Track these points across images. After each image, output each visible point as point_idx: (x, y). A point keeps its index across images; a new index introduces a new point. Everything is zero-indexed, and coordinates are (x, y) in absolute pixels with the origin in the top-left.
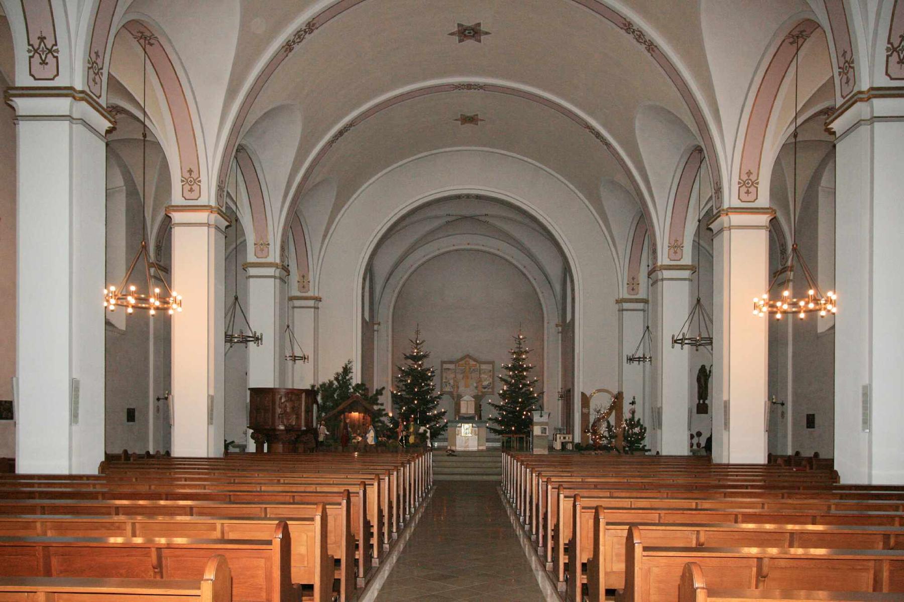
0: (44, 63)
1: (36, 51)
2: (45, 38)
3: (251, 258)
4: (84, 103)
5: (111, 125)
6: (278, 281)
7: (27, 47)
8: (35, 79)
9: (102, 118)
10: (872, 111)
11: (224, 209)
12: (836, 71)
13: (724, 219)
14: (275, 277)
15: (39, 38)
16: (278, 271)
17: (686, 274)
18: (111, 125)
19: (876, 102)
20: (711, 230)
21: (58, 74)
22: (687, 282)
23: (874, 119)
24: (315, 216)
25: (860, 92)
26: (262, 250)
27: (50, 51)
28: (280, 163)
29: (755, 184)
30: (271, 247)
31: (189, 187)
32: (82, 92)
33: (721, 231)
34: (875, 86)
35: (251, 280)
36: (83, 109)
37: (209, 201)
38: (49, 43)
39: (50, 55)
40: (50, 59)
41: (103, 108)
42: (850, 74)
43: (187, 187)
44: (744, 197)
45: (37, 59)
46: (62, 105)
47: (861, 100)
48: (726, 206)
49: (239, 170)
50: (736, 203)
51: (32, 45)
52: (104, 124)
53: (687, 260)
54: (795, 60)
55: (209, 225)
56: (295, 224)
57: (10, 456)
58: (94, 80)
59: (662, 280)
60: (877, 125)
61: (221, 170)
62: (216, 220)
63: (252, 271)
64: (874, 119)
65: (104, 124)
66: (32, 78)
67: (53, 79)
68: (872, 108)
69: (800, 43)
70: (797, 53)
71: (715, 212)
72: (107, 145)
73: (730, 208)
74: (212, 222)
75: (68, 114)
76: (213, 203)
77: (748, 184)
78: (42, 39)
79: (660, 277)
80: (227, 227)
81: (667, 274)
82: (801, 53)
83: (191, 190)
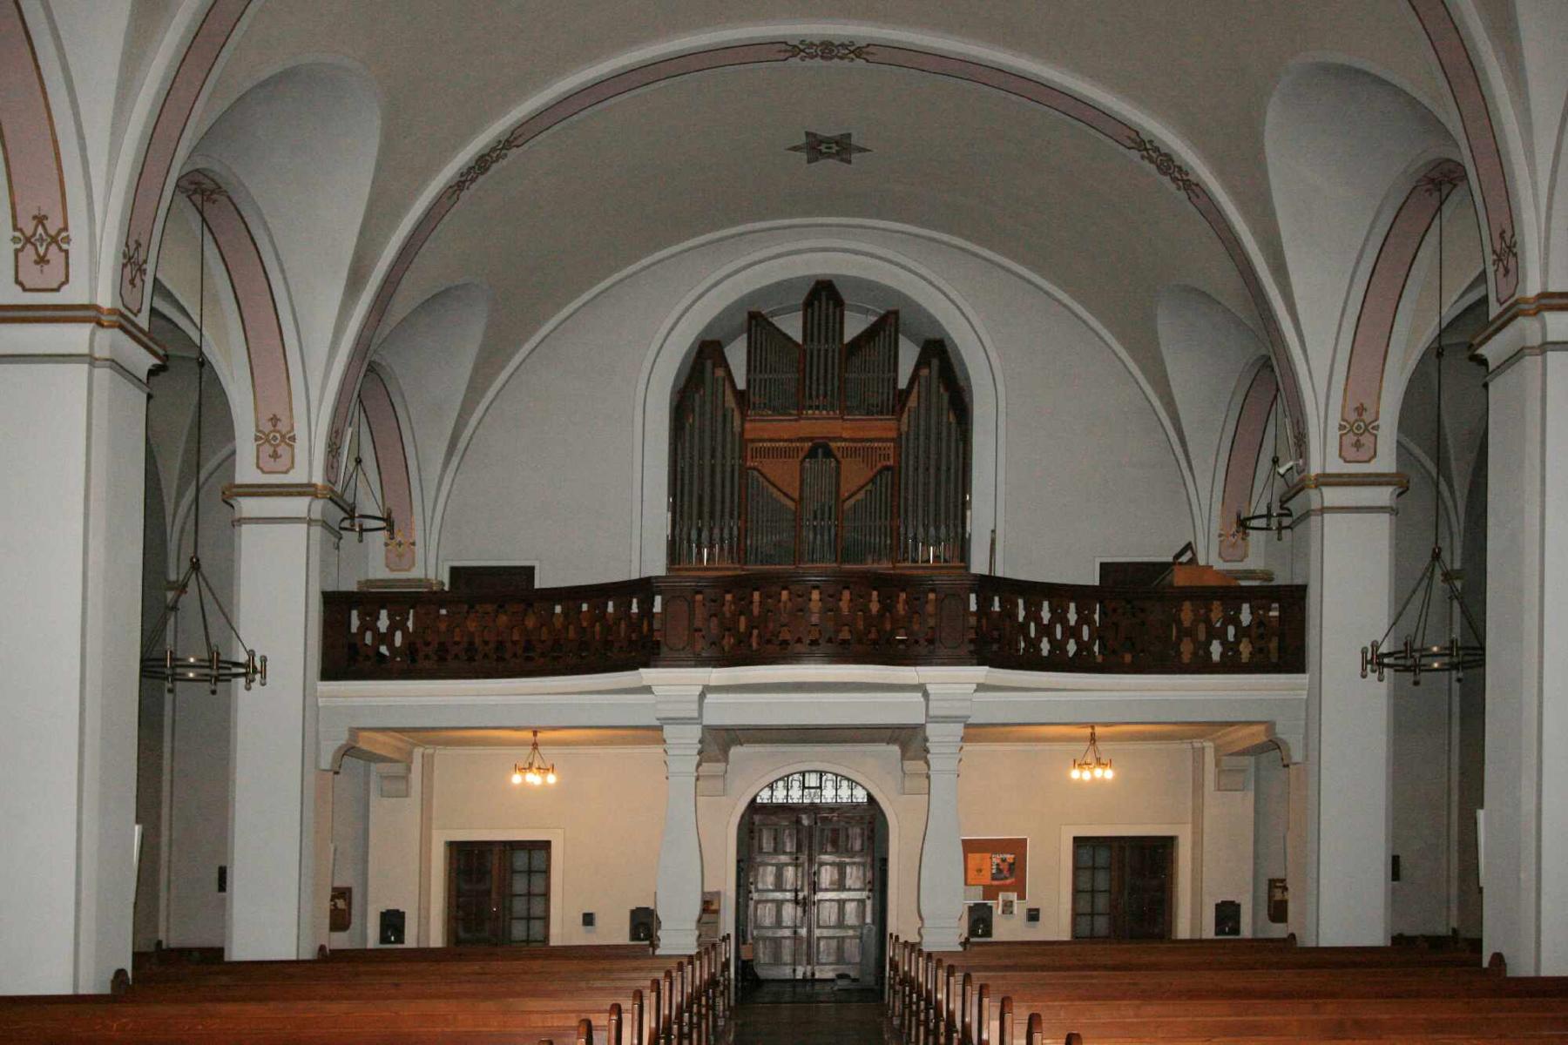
0: (42, 260)
1: (28, 240)
2: (46, 217)
3: (247, 472)
4: (117, 331)
5: (157, 362)
6: (317, 531)
7: (10, 233)
8: (25, 289)
9: (134, 345)
10: (1544, 334)
11: (143, 321)
12: (1490, 258)
13: (1314, 498)
14: (91, 359)
15: (35, 217)
16: (318, 505)
17: (1383, 495)
18: (157, 362)
19: (1551, 318)
20: (1483, 362)
21: (67, 281)
22: (1385, 517)
23: (1545, 347)
24: (434, 381)
25: (1526, 301)
26: (400, 556)
27: (54, 240)
28: (322, 227)
29: (1371, 428)
30: (301, 446)
31: (271, 450)
32: (113, 311)
33: (1307, 515)
34: (1552, 289)
35: (244, 527)
36: (109, 341)
37: (93, 290)
38: (53, 226)
39: (54, 248)
40: (54, 254)
41: (141, 330)
42: (1512, 261)
43: (268, 449)
44: (1351, 453)
45: (29, 254)
46: (76, 337)
47: (1525, 313)
48: (1315, 469)
49: (208, 236)
50: (1336, 466)
51: (21, 230)
52: (144, 361)
53: (1386, 462)
54: (1437, 221)
55: (310, 522)
56: (369, 387)
57: (217, 944)
58: (132, 282)
59: (1323, 510)
60: (1551, 356)
61: (336, 410)
62: (113, 347)
63: (248, 506)
64: (1545, 347)
65: (144, 361)
66: (19, 288)
67: (57, 290)
68: (1544, 327)
69: (1445, 192)
70: (1439, 209)
71: (1494, 310)
72: (149, 397)
73: (1325, 475)
74: (316, 515)
75: (85, 351)
76: (318, 479)
77: (1358, 429)
78: (40, 220)
79: (1315, 505)
80: (152, 372)
81: (1332, 496)
82: (1447, 210)
83: (275, 456)
